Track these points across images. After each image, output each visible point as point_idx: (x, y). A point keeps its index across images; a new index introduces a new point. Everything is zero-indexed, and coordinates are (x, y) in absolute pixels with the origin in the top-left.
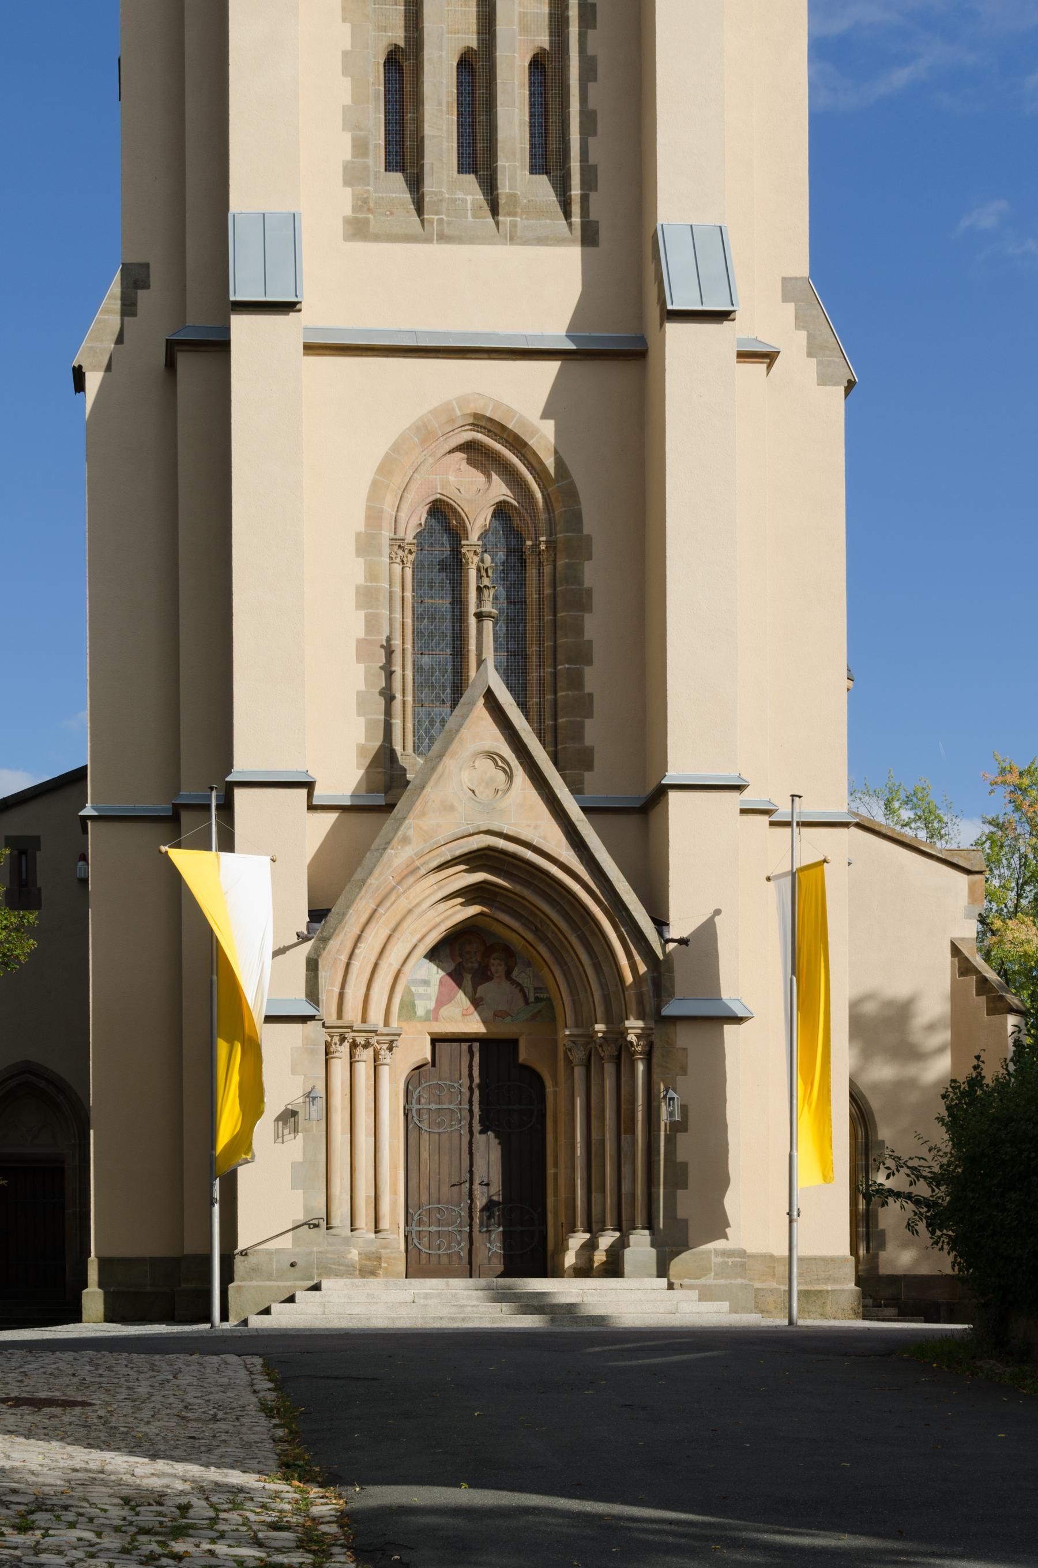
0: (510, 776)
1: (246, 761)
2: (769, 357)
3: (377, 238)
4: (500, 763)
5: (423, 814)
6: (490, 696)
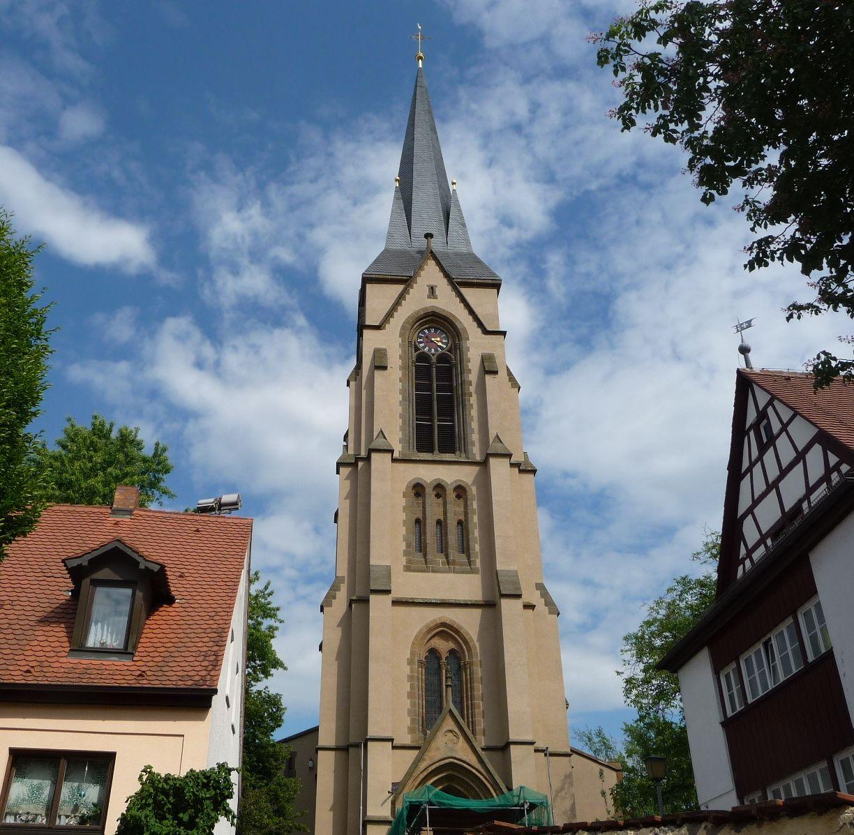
0: (458, 738)
1: (372, 732)
3: (414, 571)
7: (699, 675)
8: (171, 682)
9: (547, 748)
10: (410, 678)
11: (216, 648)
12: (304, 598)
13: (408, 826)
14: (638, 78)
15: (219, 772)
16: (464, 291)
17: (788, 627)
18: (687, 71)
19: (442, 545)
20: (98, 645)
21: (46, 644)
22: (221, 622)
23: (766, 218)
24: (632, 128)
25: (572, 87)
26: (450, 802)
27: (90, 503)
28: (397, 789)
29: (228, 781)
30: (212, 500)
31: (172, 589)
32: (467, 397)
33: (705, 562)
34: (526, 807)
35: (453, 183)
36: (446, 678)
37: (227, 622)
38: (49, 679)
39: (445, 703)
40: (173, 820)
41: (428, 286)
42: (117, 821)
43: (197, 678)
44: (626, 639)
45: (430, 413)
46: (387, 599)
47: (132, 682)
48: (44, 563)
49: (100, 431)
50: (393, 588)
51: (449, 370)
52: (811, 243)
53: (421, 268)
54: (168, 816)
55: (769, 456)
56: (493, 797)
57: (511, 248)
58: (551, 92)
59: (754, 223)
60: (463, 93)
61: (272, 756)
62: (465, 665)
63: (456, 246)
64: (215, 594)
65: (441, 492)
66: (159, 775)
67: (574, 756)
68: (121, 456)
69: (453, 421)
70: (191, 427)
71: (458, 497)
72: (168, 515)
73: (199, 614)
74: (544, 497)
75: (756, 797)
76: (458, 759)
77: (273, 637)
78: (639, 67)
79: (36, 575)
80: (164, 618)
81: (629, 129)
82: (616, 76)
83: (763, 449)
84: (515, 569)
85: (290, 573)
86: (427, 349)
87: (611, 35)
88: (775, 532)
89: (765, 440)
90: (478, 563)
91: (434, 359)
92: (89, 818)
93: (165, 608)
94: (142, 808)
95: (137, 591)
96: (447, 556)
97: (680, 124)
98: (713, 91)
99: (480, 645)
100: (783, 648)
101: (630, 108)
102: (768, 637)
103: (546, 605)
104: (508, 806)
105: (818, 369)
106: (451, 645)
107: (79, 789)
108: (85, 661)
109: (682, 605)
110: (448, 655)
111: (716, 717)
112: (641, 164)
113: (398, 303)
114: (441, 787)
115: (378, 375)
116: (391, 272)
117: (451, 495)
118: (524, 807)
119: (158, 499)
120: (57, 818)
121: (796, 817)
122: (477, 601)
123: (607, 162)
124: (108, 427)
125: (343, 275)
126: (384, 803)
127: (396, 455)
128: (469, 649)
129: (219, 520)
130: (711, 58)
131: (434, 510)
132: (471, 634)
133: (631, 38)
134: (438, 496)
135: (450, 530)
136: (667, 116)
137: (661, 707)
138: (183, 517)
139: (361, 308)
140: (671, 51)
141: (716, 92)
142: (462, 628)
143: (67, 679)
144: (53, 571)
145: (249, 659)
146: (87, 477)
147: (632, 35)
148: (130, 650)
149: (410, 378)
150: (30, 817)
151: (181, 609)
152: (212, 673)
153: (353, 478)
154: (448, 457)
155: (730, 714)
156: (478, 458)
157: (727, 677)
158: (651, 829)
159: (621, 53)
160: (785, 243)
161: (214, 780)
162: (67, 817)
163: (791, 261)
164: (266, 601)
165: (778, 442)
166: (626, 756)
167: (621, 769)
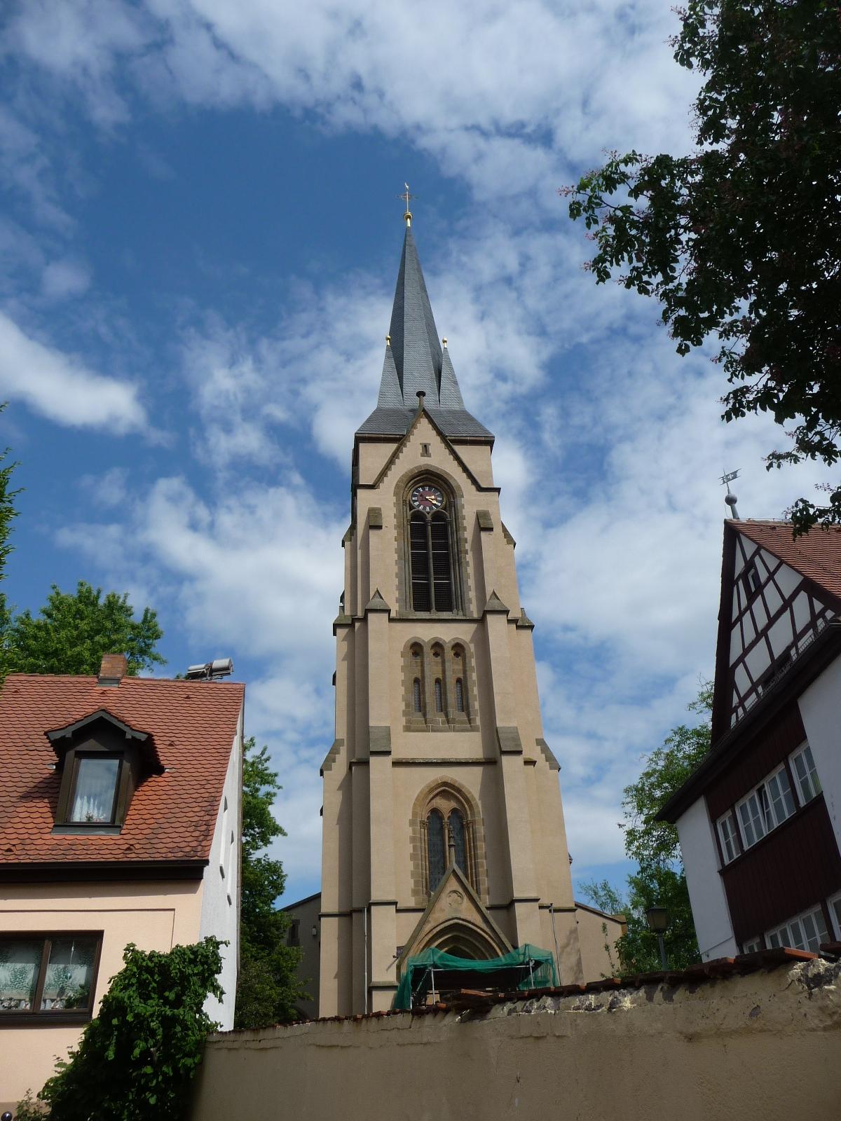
1: (375, 896)
2: (533, 763)
6: (454, 871)
7: (697, 824)
8: (161, 855)
9: (551, 904)
10: (413, 840)
11: (207, 818)
12: (307, 761)
13: (414, 989)
14: (611, 231)
15: (207, 946)
16: (457, 448)
17: (779, 773)
18: (657, 222)
19: (441, 701)
20: (84, 820)
21: (28, 820)
22: (213, 790)
23: (742, 370)
24: (607, 281)
26: (455, 964)
27: (77, 673)
28: (402, 952)
29: (217, 956)
30: (203, 666)
31: (161, 758)
33: (701, 712)
34: (531, 964)
35: (444, 342)
36: (449, 838)
37: (219, 790)
38: (31, 857)
39: (448, 863)
40: (159, 998)
42: (100, 1003)
43: (188, 849)
44: (626, 791)
45: (427, 571)
46: (388, 760)
47: (120, 856)
48: (27, 736)
49: (87, 599)
50: (393, 749)
51: (445, 528)
52: (783, 391)
53: (414, 426)
54: (153, 995)
55: (758, 605)
56: (498, 956)
57: (507, 403)
58: (539, 245)
59: (732, 374)
60: (453, 245)
61: (273, 925)
62: (468, 824)
63: (448, 404)
64: (206, 762)
65: (439, 650)
66: (143, 952)
67: (579, 911)
68: (109, 625)
69: (449, 579)
70: (186, 591)
71: (457, 655)
72: (156, 683)
73: (190, 783)
74: (542, 651)
75: (754, 944)
76: (447, 921)
77: (271, 803)
78: (612, 219)
79: (18, 749)
80: (153, 788)
81: (604, 281)
82: (589, 228)
83: (751, 598)
84: (515, 725)
85: (292, 736)
86: (421, 507)
87: (582, 187)
88: (766, 679)
89: (753, 589)
90: (478, 722)
91: (429, 517)
92: (76, 1000)
93: (155, 778)
94: (125, 988)
95: (124, 761)
96: (447, 715)
97: (653, 276)
98: (684, 243)
99: (482, 804)
100: (775, 794)
101: (604, 261)
102: (761, 784)
104: (512, 965)
105: (796, 516)
106: (453, 804)
107: (65, 970)
108: (70, 836)
109: (680, 755)
111: (713, 866)
112: (630, 317)
113: (391, 462)
114: (446, 949)
115: (373, 534)
116: (384, 431)
117: (449, 653)
119: (148, 666)
120: (42, 1003)
121: (747, 974)
122: (477, 759)
123: (598, 314)
124: (96, 594)
125: (337, 431)
126: (389, 967)
127: (393, 614)
128: (471, 806)
129: (211, 686)
130: (682, 210)
131: (432, 670)
132: (473, 793)
133: (602, 191)
134: (436, 654)
135: (448, 688)
136: (641, 268)
137: (662, 858)
138: (173, 684)
139: (356, 468)
140: (642, 203)
141: (687, 244)
143: (51, 857)
144: (36, 744)
145: (246, 827)
146: (73, 645)
147: (604, 187)
148: (117, 823)
149: (406, 537)
150: (13, 1003)
151: (171, 779)
152: (203, 844)
153: (350, 638)
154: (445, 615)
155: (727, 862)
156: (475, 616)
157: (724, 825)
158: (611, 992)
159: (594, 206)
160: (758, 392)
161: (202, 955)
162: (53, 1001)
163: (764, 409)
164: (263, 767)
165: (766, 591)
166: (631, 907)
167: (628, 921)
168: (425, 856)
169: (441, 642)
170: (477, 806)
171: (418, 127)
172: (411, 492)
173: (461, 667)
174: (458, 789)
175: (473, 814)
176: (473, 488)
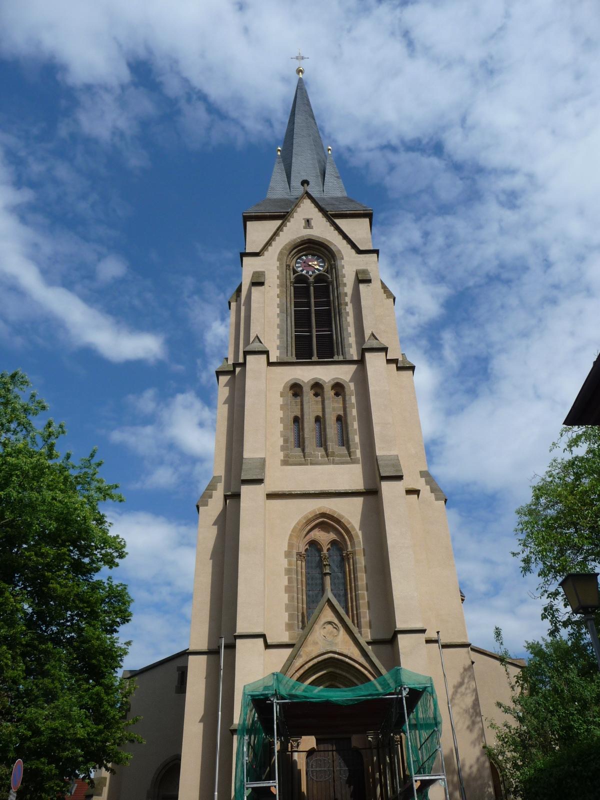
1: (240, 629)
2: (416, 492)
3: (291, 465)
4: (334, 626)
5: (352, 653)
6: (329, 601)
10: (288, 571)
16: (338, 221)
25: (449, 219)
32: (343, 307)
34: (404, 693)
41: (304, 219)
56: (369, 680)
57: (414, 328)
58: (439, 223)
62: (348, 555)
65: (319, 391)
69: (331, 331)
70: (198, 469)
71: (337, 394)
86: (304, 272)
91: (311, 279)
96: (326, 450)
103: (432, 492)
106: (332, 536)
110: (329, 546)
113: (276, 234)
117: (329, 393)
118: (402, 694)
127: (273, 359)
128: (351, 537)
142: (343, 517)
149: (288, 295)
156: (355, 358)
168: (302, 590)
169: (321, 382)
170: (358, 536)
171: (349, 149)
172: (295, 259)
173: (341, 405)
174: (337, 519)
175: (353, 545)
176: (353, 251)
